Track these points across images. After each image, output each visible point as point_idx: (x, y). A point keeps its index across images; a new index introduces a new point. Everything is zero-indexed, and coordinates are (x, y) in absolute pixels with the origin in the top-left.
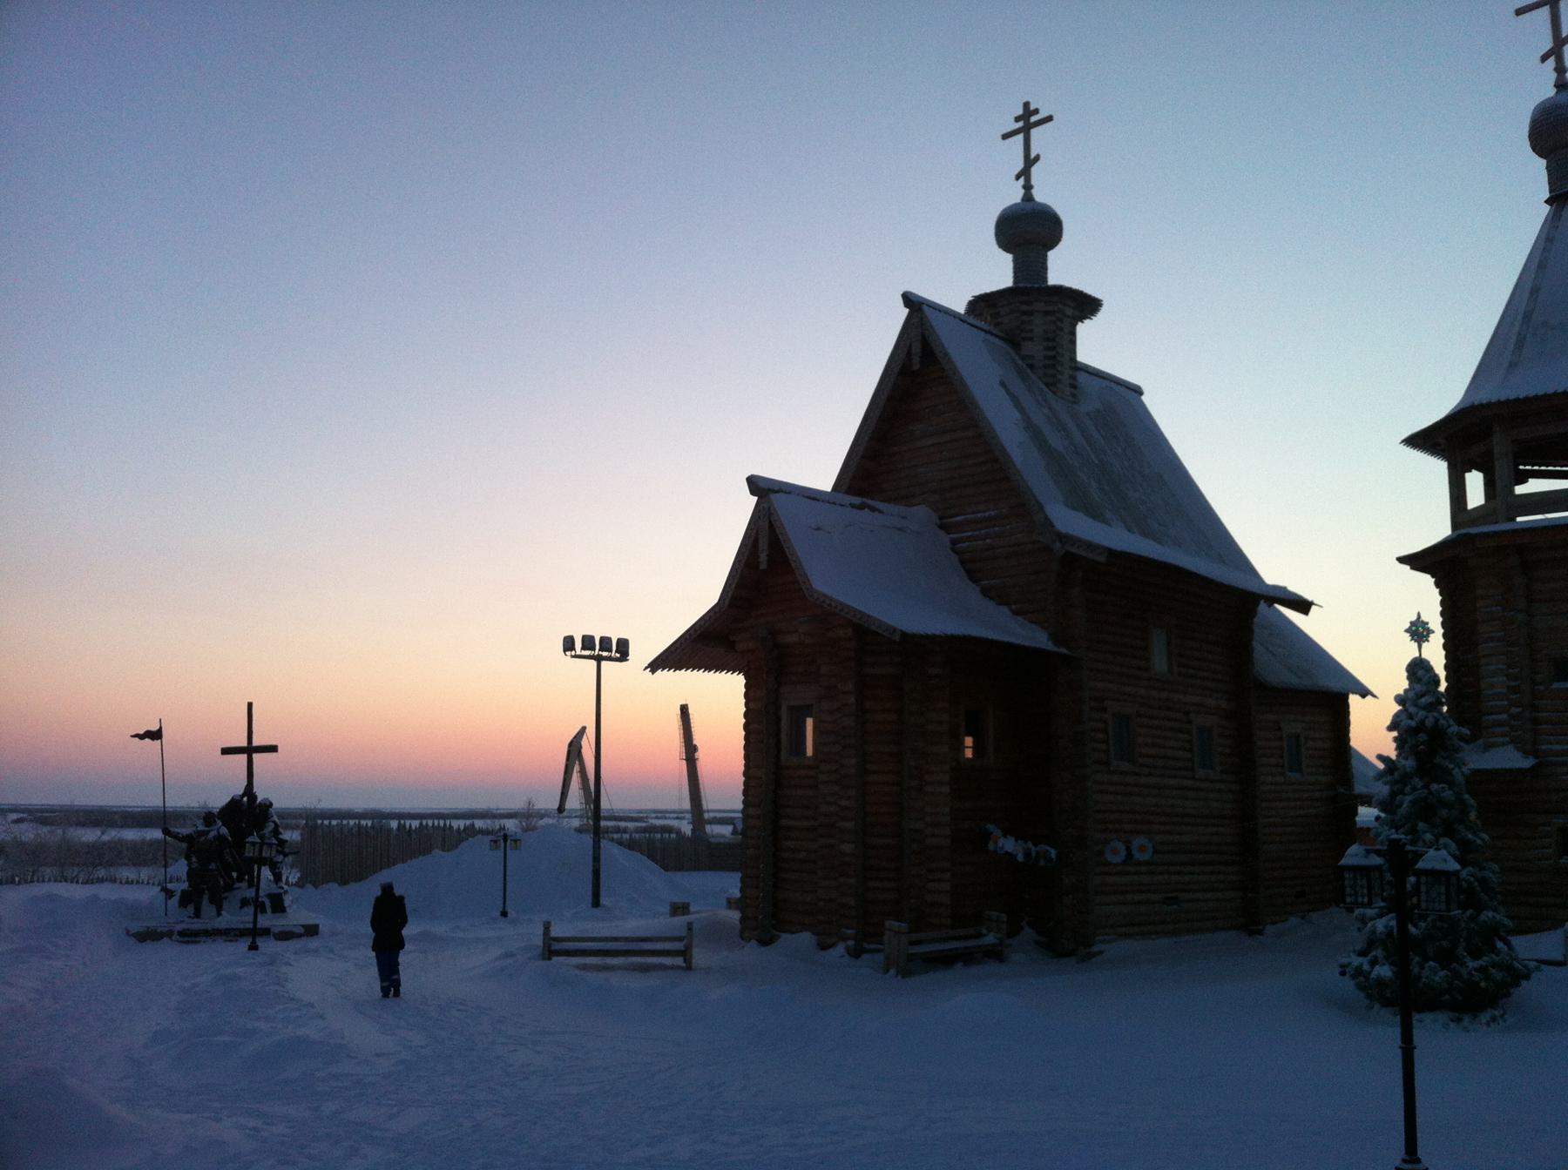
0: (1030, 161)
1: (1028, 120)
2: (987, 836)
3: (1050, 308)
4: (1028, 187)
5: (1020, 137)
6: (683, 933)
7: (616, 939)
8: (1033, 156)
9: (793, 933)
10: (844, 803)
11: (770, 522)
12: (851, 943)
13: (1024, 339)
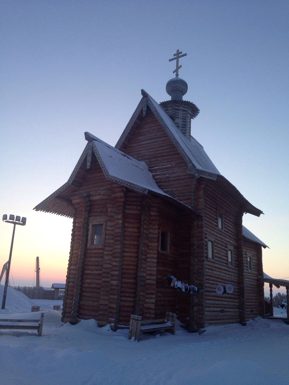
0: (178, 67)
1: (178, 55)
2: (170, 280)
4: (177, 75)
5: (176, 60)
6: (39, 318)
7: (6, 320)
8: (179, 65)
9: (86, 319)
10: (114, 264)
12: (113, 324)
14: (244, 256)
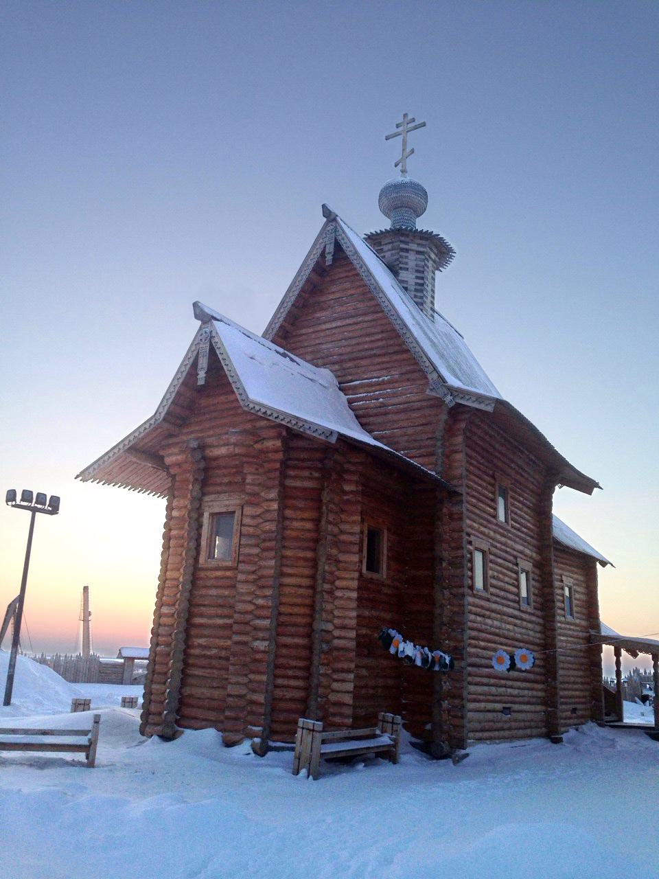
2: (389, 640)
3: (422, 249)
6: (88, 725)
9: (196, 729)
10: (260, 602)
11: (211, 345)
12: (257, 740)
13: (401, 268)
14: (557, 584)
